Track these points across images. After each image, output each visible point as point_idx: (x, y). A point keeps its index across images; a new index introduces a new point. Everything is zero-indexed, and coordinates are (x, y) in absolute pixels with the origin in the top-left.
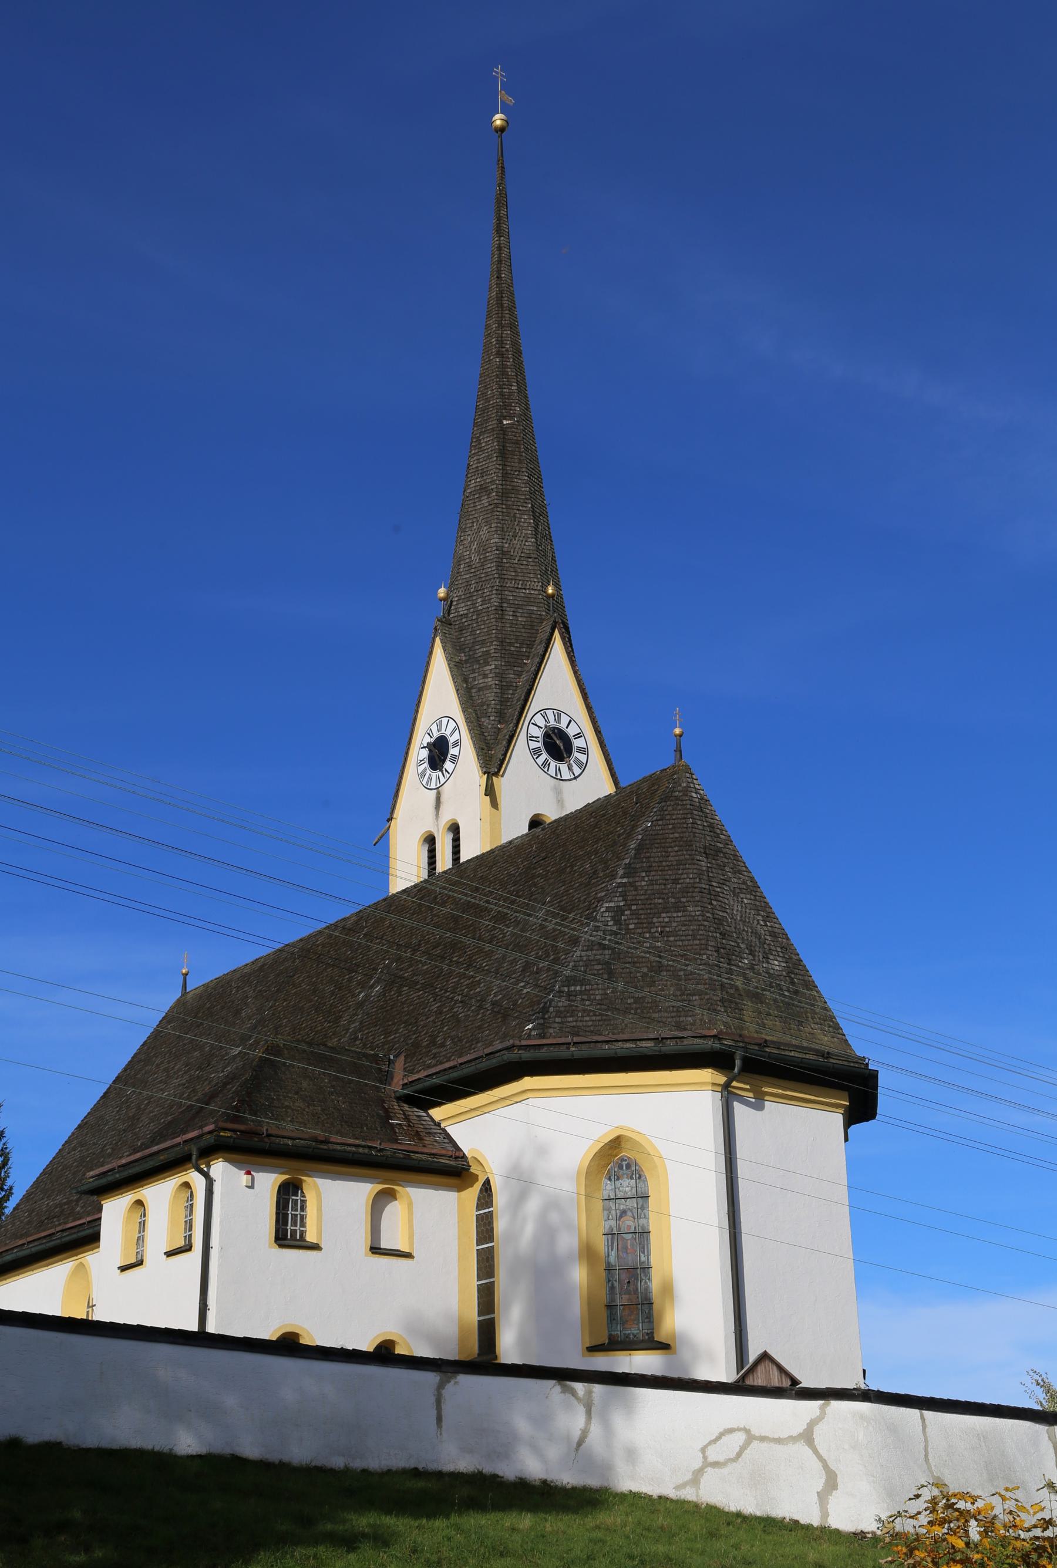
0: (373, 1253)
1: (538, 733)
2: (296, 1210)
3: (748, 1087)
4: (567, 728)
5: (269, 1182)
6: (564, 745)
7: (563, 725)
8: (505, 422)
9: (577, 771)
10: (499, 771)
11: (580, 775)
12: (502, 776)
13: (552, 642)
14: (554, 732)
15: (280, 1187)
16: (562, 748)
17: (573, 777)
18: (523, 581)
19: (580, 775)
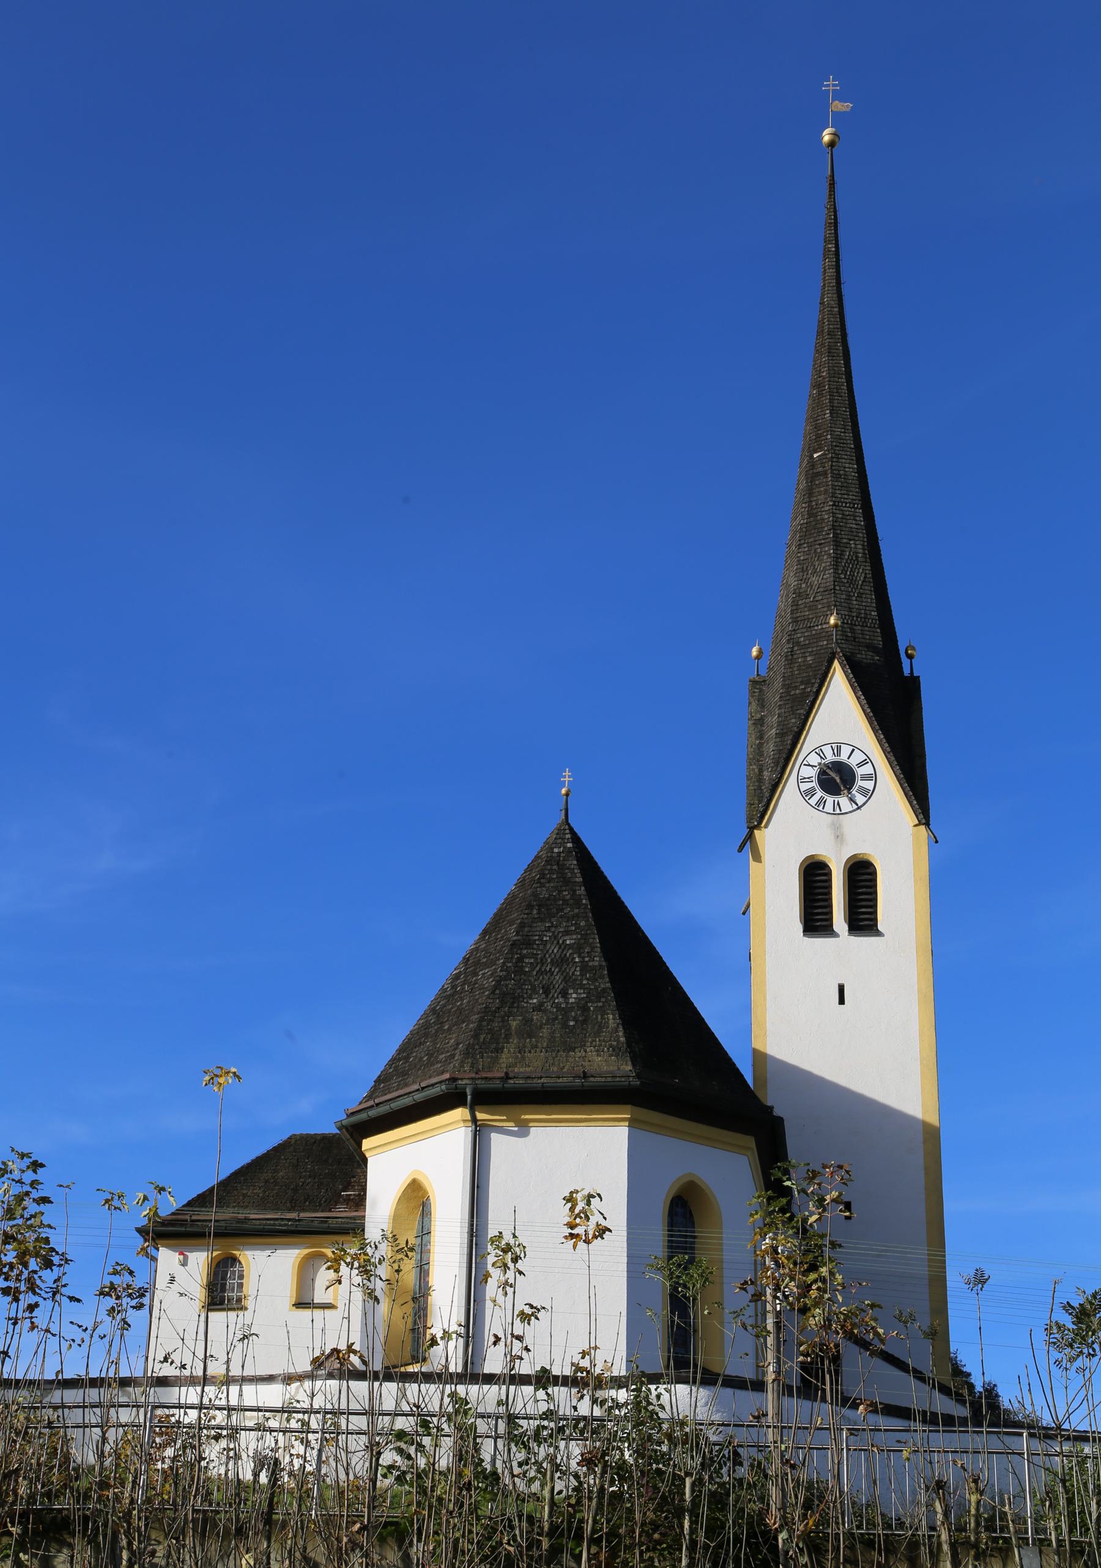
0: (297, 1308)
1: (812, 773)
2: (234, 1279)
3: (505, 1118)
4: (848, 758)
5: (200, 1260)
6: (840, 778)
7: (844, 757)
8: (815, 456)
9: (860, 799)
10: (760, 822)
11: (864, 804)
12: (766, 826)
13: (830, 675)
14: (828, 767)
15: (672, 1201)
16: (838, 781)
17: (855, 807)
18: (874, 627)
19: (864, 804)
